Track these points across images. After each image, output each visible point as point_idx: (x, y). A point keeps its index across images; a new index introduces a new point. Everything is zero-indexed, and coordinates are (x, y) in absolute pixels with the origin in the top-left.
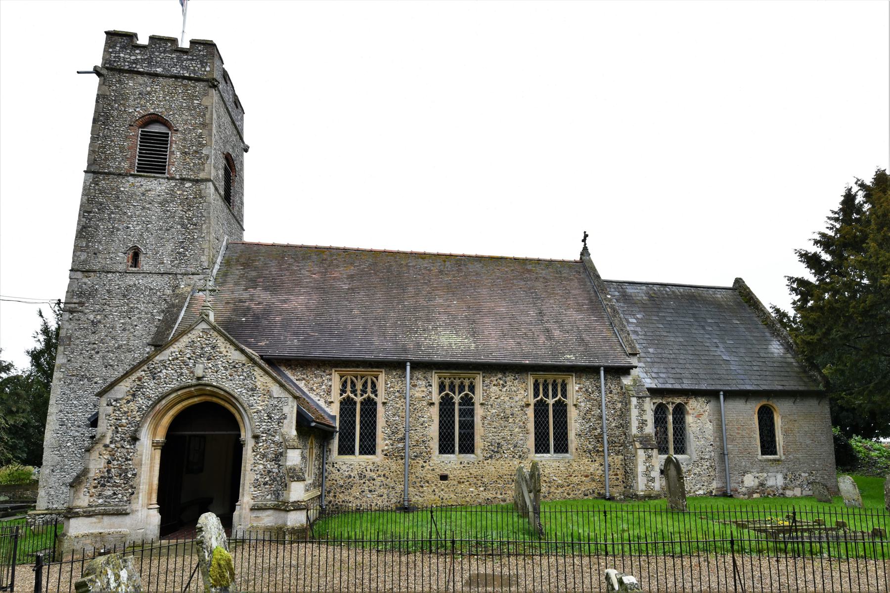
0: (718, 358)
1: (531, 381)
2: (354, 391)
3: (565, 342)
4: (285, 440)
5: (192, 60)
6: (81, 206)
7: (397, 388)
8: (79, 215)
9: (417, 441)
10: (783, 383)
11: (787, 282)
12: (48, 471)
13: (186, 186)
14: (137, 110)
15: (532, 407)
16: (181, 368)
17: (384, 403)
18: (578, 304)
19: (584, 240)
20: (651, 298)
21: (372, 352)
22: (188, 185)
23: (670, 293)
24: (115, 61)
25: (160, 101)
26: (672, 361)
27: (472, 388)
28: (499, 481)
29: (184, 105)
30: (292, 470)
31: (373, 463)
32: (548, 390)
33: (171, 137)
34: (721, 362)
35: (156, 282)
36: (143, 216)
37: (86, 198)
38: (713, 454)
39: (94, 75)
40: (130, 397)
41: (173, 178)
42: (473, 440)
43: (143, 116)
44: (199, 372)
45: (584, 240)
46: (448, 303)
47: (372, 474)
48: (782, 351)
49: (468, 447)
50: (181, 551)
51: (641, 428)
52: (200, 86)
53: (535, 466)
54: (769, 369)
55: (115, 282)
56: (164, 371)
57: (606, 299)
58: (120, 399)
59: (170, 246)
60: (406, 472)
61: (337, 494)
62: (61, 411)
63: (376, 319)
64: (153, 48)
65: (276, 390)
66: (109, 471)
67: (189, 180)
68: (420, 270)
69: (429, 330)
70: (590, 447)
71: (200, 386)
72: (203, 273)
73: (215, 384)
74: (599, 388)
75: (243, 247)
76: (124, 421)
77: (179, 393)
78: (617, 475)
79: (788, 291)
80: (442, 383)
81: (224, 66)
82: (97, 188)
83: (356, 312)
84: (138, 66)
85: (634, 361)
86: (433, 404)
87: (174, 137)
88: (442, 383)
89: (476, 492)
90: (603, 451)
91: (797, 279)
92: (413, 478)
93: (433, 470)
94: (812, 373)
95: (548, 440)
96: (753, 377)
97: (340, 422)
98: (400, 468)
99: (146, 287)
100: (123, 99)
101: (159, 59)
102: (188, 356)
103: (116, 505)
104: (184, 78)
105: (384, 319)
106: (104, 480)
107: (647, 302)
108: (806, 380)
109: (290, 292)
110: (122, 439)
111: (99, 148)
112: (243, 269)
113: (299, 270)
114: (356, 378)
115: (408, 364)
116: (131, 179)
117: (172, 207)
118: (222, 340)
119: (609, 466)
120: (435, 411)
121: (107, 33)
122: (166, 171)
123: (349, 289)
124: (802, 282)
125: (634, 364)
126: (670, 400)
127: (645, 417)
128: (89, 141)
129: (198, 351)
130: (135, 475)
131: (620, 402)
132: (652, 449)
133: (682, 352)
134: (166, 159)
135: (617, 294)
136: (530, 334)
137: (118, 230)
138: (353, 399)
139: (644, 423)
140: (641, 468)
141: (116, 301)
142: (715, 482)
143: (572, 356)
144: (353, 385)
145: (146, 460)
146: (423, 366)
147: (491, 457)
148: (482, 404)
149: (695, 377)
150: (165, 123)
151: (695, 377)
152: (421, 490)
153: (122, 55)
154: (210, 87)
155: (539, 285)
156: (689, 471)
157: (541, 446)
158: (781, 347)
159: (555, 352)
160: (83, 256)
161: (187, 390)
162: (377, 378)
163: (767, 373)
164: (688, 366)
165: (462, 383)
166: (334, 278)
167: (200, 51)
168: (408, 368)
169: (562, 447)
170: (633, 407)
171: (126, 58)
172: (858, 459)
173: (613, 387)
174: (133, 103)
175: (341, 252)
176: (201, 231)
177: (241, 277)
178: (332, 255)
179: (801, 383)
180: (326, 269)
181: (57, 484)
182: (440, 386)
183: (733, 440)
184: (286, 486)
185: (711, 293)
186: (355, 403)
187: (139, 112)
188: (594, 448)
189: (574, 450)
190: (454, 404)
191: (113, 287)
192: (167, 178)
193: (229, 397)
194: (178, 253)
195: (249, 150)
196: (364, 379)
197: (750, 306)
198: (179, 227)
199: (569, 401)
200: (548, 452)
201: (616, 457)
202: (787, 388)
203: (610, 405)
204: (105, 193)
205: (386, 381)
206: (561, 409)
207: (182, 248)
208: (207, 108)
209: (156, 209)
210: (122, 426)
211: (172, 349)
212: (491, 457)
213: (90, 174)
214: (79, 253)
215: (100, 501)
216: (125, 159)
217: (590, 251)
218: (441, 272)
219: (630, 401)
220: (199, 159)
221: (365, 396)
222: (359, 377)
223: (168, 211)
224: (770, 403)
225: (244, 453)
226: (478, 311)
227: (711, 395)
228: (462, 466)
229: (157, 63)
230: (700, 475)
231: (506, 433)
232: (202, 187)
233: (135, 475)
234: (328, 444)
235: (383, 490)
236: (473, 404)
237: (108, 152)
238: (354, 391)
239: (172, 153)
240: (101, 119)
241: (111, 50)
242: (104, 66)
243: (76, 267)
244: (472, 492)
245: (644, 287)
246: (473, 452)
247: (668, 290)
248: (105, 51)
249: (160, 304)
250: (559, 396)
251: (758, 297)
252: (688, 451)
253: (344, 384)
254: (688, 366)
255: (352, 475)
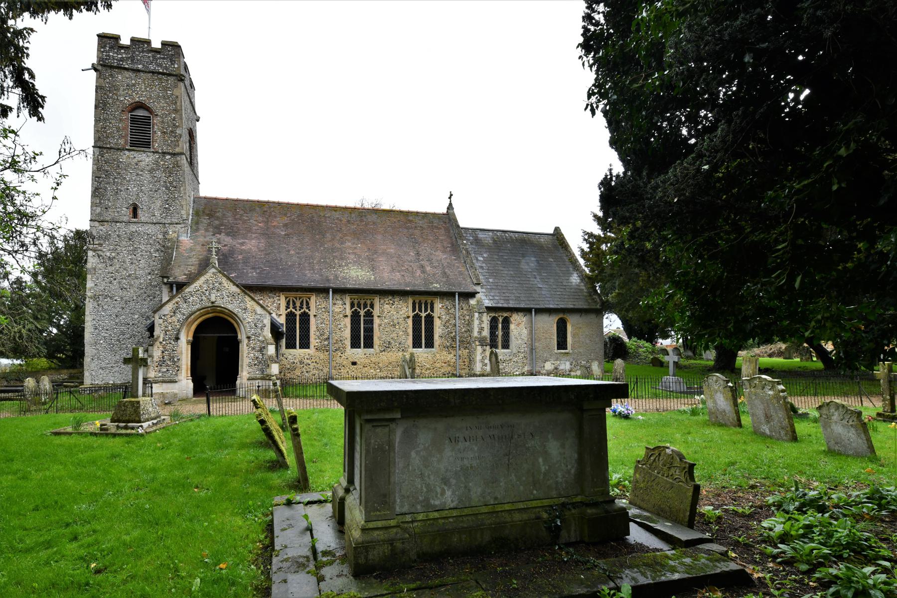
0: (534, 286)
1: (410, 301)
2: (295, 308)
3: (434, 275)
4: (266, 340)
5: (164, 58)
6: (93, 173)
7: (323, 306)
8: (92, 180)
9: (337, 340)
10: (574, 303)
11: (582, 234)
12: (89, 359)
13: (167, 158)
14: (127, 98)
15: (411, 318)
16: (201, 296)
17: (315, 316)
18: (444, 247)
19: (450, 198)
20: (495, 241)
21: (306, 282)
22: (168, 157)
23: (509, 238)
24: (106, 59)
25: (143, 92)
26: (504, 288)
27: (372, 306)
28: (389, 366)
29: (161, 95)
30: (270, 357)
31: (309, 354)
32: (421, 307)
33: (153, 120)
34: (536, 289)
35: (151, 229)
36: (138, 181)
37: (96, 166)
38: (526, 349)
39: (93, 70)
40: (172, 314)
41: (157, 152)
42: (373, 339)
43: (132, 104)
44: (213, 299)
45: (450, 198)
46: (355, 246)
47: (308, 361)
48: (578, 281)
49: (369, 344)
50: (218, 401)
51: (480, 333)
52: (171, 80)
53: (412, 355)
54: (568, 293)
55: (122, 229)
56: (192, 298)
57: (463, 244)
58: (167, 315)
59: (159, 203)
60: (330, 361)
61: (286, 374)
62: (94, 320)
63: (307, 257)
64: (134, 48)
65: (259, 310)
66: (163, 357)
67: (169, 154)
68: (334, 220)
69: (342, 266)
70: (448, 344)
71: (214, 307)
72: (184, 223)
73: (222, 306)
74: (454, 306)
75: (205, 201)
76: (170, 328)
77: (202, 311)
78: (464, 362)
79: (582, 240)
80: (353, 302)
81: (185, 60)
82: (103, 159)
83: (292, 252)
84: (124, 63)
85: (478, 289)
86: (347, 316)
87: (156, 120)
88: (353, 302)
89: (375, 373)
90: (456, 347)
91: (588, 233)
92: (334, 364)
93: (347, 359)
94: (594, 297)
95: (421, 339)
96: (556, 299)
97: (286, 327)
98: (326, 357)
99: (144, 233)
100: (115, 90)
101: (139, 58)
102: (205, 289)
103: (169, 377)
104: (159, 73)
105: (312, 257)
106: (162, 363)
107: (492, 245)
108: (590, 301)
109: (245, 237)
110: (170, 339)
111: (102, 128)
112: (209, 219)
113: (249, 220)
114: (296, 298)
115: (331, 290)
116: (126, 152)
117: (158, 174)
118: (225, 279)
119: (460, 356)
120: (348, 321)
121: (99, 36)
122: (151, 146)
123: (285, 235)
124: (591, 235)
125: (478, 291)
126: (500, 314)
127: (483, 326)
128: (93, 123)
129: (211, 286)
130: (179, 359)
131: (468, 315)
132: (486, 346)
133: (512, 281)
134: (150, 137)
135: (471, 238)
136: (410, 269)
137: (121, 191)
138: (294, 313)
139: (482, 329)
140: (479, 357)
141: (124, 243)
142: (526, 367)
143: (437, 285)
144: (294, 303)
145: (184, 351)
146: (340, 291)
147: (384, 351)
148: (379, 316)
149: (518, 299)
150: (147, 109)
151: (518, 299)
152: (339, 371)
153: (111, 54)
154: (179, 80)
155: (417, 232)
156: (510, 360)
157: (417, 344)
158: (578, 278)
159: (427, 282)
160: (98, 210)
161: (204, 310)
162: (310, 299)
163: (566, 297)
164: (514, 291)
165: (365, 302)
166: (274, 226)
167: (169, 51)
168: (331, 292)
169: (430, 344)
170: (475, 319)
171: (115, 56)
172: (629, 353)
173: (463, 305)
174: (123, 93)
175: (276, 205)
176: (179, 192)
177: (209, 225)
178: (270, 207)
179: (586, 303)
180: (267, 219)
181: (96, 368)
182: (351, 304)
183: (539, 340)
184: (268, 366)
185: (537, 237)
186: (296, 315)
187: (128, 101)
188: (451, 345)
189: (438, 346)
190: (360, 316)
191: (122, 233)
192: (153, 152)
193: (231, 314)
194: (165, 208)
195: (200, 119)
196: (301, 300)
197: (562, 248)
198: (164, 189)
199: (435, 315)
200: (421, 347)
201: (464, 351)
202: (576, 307)
203: (461, 317)
204: (109, 163)
205: (316, 301)
206: (430, 320)
207: (168, 204)
208: (177, 97)
209: (147, 176)
210: (169, 331)
211: (195, 285)
212: (384, 351)
213: (97, 149)
214: (95, 208)
215: (160, 374)
216: (121, 137)
217: (453, 206)
218: (348, 221)
219: (474, 315)
220: (175, 137)
221: (302, 311)
222: (298, 298)
223: (155, 177)
224: (565, 316)
225: (240, 347)
226: (376, 253)
227: (527, 311)
228: (365, 356)
229: (138, 61)
230: (517, 362)
231: (394, 335)
232: (178, 158)
233: (179, 359)
234: (280, 342)
235: (315, 372)
236: (373, 316)
237: (108, 132)
238: (295, 308)
239: (155, 132)
240: (101, 105)
241: (102, 50)
242: (99, 63)
243: (94, 218)
244: (372, 373)
245: (491, 233)
246: (372, 347)
247: (507, 235)
248: (98, 50)
249: (155, 245)
250: (429, 311)
251: (568, 242)
252: (511, 347)
253: (288, 303)
254: (514, 291)
255: (295, 361)
